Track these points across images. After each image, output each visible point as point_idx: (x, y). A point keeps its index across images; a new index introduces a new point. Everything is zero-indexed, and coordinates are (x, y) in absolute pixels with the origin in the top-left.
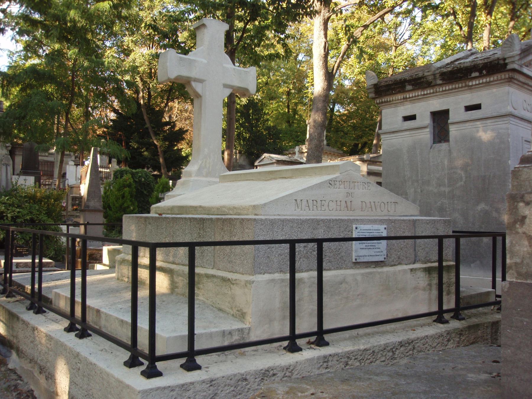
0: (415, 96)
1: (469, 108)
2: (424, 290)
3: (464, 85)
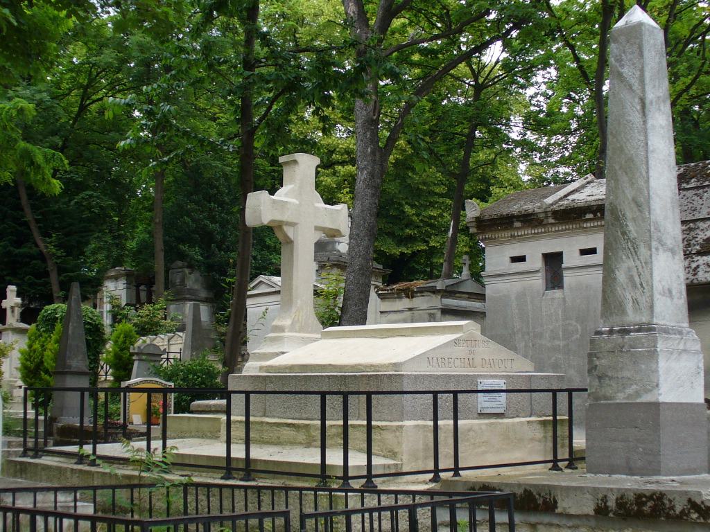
0: (525, 235)
1: (584, 252)
2: (540, 441)
3: (578, 226)
